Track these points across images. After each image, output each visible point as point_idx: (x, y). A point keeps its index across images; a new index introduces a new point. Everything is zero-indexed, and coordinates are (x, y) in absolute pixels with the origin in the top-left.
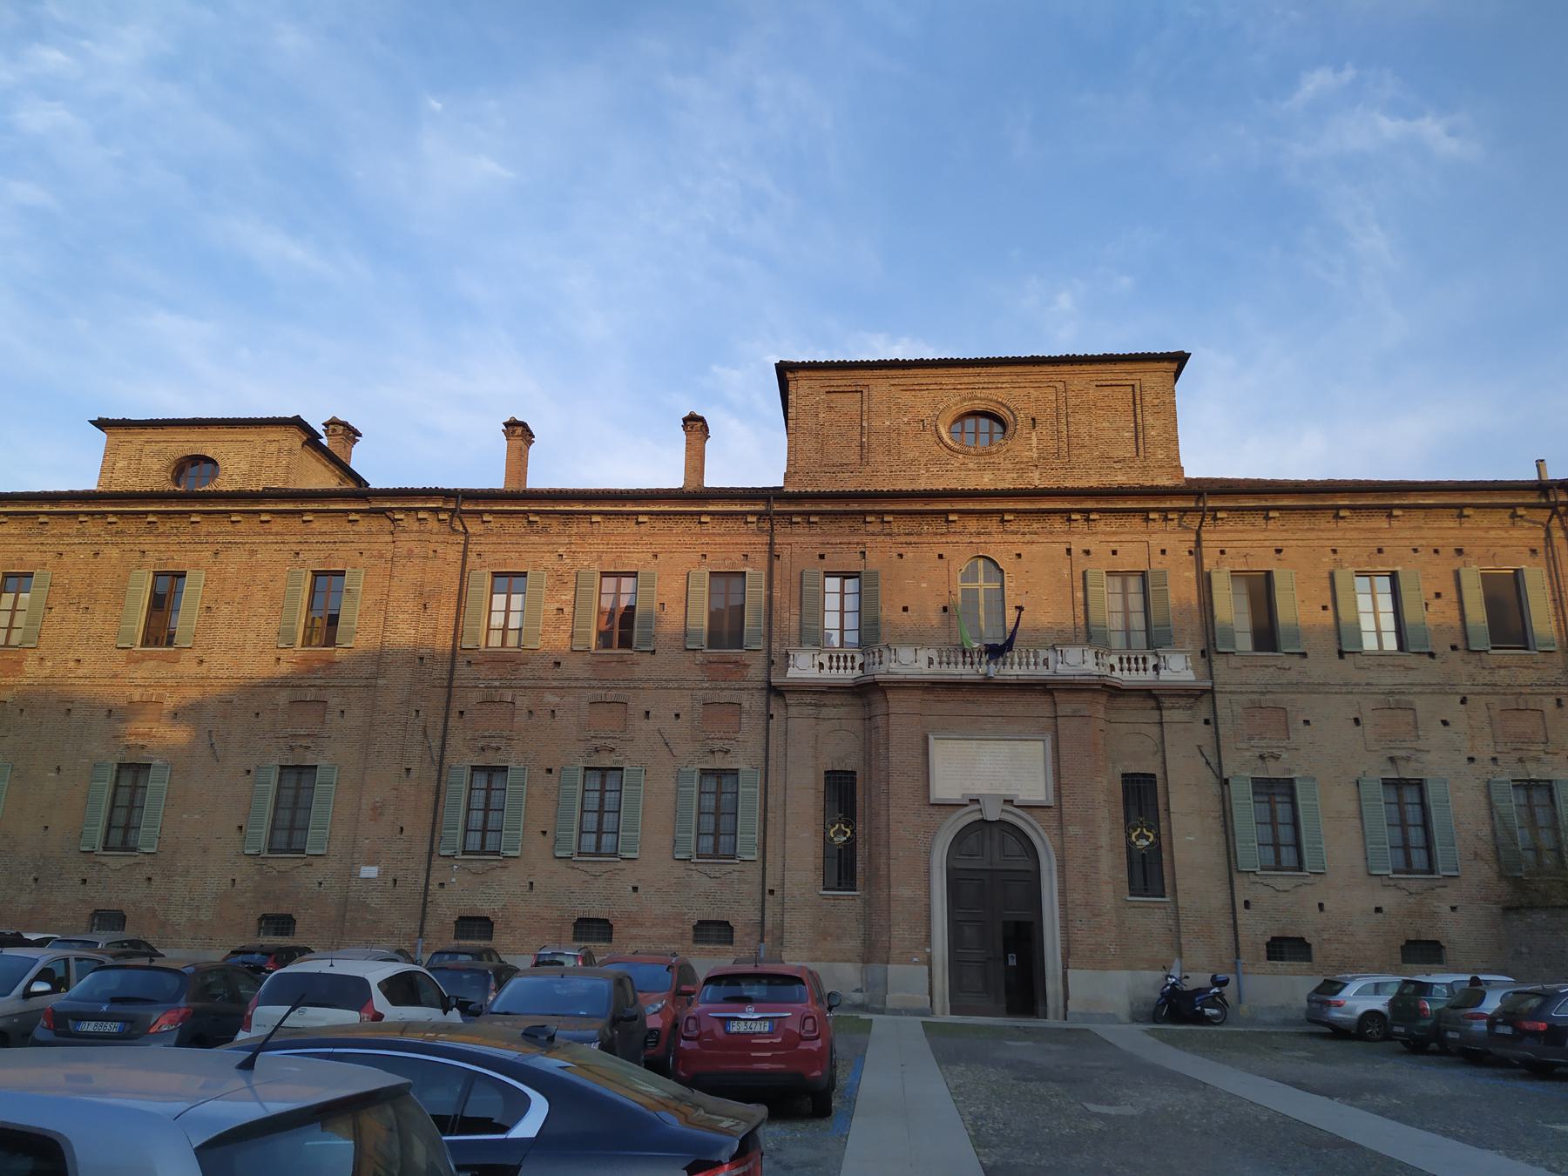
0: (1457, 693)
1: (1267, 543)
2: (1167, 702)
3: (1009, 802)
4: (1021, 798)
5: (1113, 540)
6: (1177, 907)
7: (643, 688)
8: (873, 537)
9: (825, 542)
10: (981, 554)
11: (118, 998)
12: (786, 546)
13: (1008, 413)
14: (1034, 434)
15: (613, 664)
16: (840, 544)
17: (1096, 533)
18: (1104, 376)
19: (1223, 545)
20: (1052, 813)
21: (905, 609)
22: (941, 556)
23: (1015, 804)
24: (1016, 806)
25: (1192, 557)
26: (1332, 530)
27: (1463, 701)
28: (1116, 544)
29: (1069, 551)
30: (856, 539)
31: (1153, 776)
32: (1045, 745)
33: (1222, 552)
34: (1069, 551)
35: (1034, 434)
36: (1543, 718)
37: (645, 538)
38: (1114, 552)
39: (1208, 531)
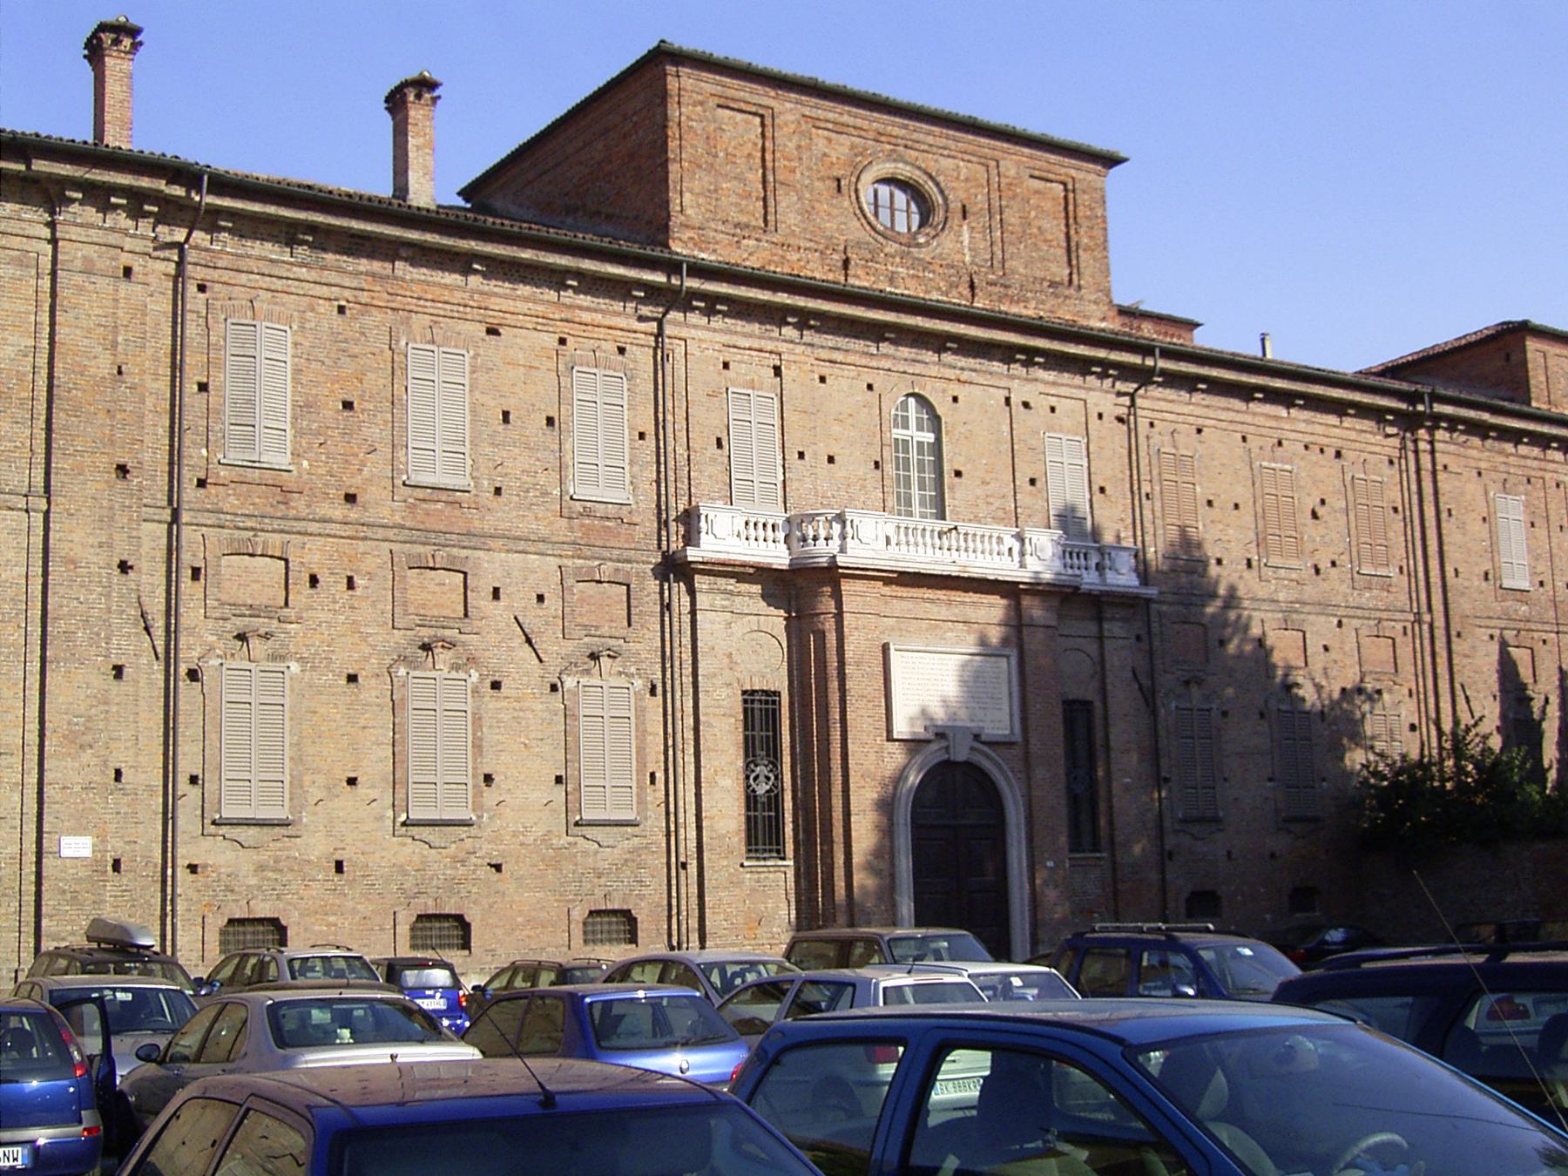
0: (1335, 615)
1: (1191, 420)
2: (1108, 613)
3: (977, 737)
4: (990, 731)
5: (1052, 392)
6: (1114, 863)
7: (365, 539)
8: (791, 346)
9: (731, 343)
10: (916, 390)
11: (1160, 1042)
12: (677, 341)
13: (935, 189)
14: (965, 227)
15: (440, 506)
16: (750, 349)
17: (1036, 380)
18: (1039, 164)
19: (1200, 421)
20: (1017, 751)
21: (831, 460)
22: (870, 387)
23: (983, 738)
24: (984, 743)
25: (1395, 470)
26: (618, 314)
27: (1340, 624)
28: (1054, 399)
29: (1008, 401)
30: (770, 346)
31: (1091, 703)
32: (1009, 663)
33: (1280, 444)
34: (1008, 401)
35: (965, 227)
36: (465, 579)
37: (476, 296)
38: (1053, 409)
39: (676, 323)
